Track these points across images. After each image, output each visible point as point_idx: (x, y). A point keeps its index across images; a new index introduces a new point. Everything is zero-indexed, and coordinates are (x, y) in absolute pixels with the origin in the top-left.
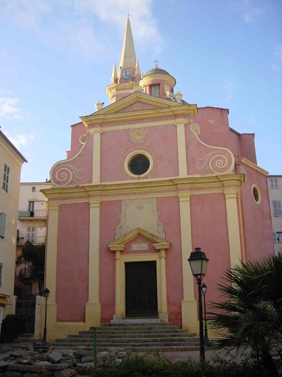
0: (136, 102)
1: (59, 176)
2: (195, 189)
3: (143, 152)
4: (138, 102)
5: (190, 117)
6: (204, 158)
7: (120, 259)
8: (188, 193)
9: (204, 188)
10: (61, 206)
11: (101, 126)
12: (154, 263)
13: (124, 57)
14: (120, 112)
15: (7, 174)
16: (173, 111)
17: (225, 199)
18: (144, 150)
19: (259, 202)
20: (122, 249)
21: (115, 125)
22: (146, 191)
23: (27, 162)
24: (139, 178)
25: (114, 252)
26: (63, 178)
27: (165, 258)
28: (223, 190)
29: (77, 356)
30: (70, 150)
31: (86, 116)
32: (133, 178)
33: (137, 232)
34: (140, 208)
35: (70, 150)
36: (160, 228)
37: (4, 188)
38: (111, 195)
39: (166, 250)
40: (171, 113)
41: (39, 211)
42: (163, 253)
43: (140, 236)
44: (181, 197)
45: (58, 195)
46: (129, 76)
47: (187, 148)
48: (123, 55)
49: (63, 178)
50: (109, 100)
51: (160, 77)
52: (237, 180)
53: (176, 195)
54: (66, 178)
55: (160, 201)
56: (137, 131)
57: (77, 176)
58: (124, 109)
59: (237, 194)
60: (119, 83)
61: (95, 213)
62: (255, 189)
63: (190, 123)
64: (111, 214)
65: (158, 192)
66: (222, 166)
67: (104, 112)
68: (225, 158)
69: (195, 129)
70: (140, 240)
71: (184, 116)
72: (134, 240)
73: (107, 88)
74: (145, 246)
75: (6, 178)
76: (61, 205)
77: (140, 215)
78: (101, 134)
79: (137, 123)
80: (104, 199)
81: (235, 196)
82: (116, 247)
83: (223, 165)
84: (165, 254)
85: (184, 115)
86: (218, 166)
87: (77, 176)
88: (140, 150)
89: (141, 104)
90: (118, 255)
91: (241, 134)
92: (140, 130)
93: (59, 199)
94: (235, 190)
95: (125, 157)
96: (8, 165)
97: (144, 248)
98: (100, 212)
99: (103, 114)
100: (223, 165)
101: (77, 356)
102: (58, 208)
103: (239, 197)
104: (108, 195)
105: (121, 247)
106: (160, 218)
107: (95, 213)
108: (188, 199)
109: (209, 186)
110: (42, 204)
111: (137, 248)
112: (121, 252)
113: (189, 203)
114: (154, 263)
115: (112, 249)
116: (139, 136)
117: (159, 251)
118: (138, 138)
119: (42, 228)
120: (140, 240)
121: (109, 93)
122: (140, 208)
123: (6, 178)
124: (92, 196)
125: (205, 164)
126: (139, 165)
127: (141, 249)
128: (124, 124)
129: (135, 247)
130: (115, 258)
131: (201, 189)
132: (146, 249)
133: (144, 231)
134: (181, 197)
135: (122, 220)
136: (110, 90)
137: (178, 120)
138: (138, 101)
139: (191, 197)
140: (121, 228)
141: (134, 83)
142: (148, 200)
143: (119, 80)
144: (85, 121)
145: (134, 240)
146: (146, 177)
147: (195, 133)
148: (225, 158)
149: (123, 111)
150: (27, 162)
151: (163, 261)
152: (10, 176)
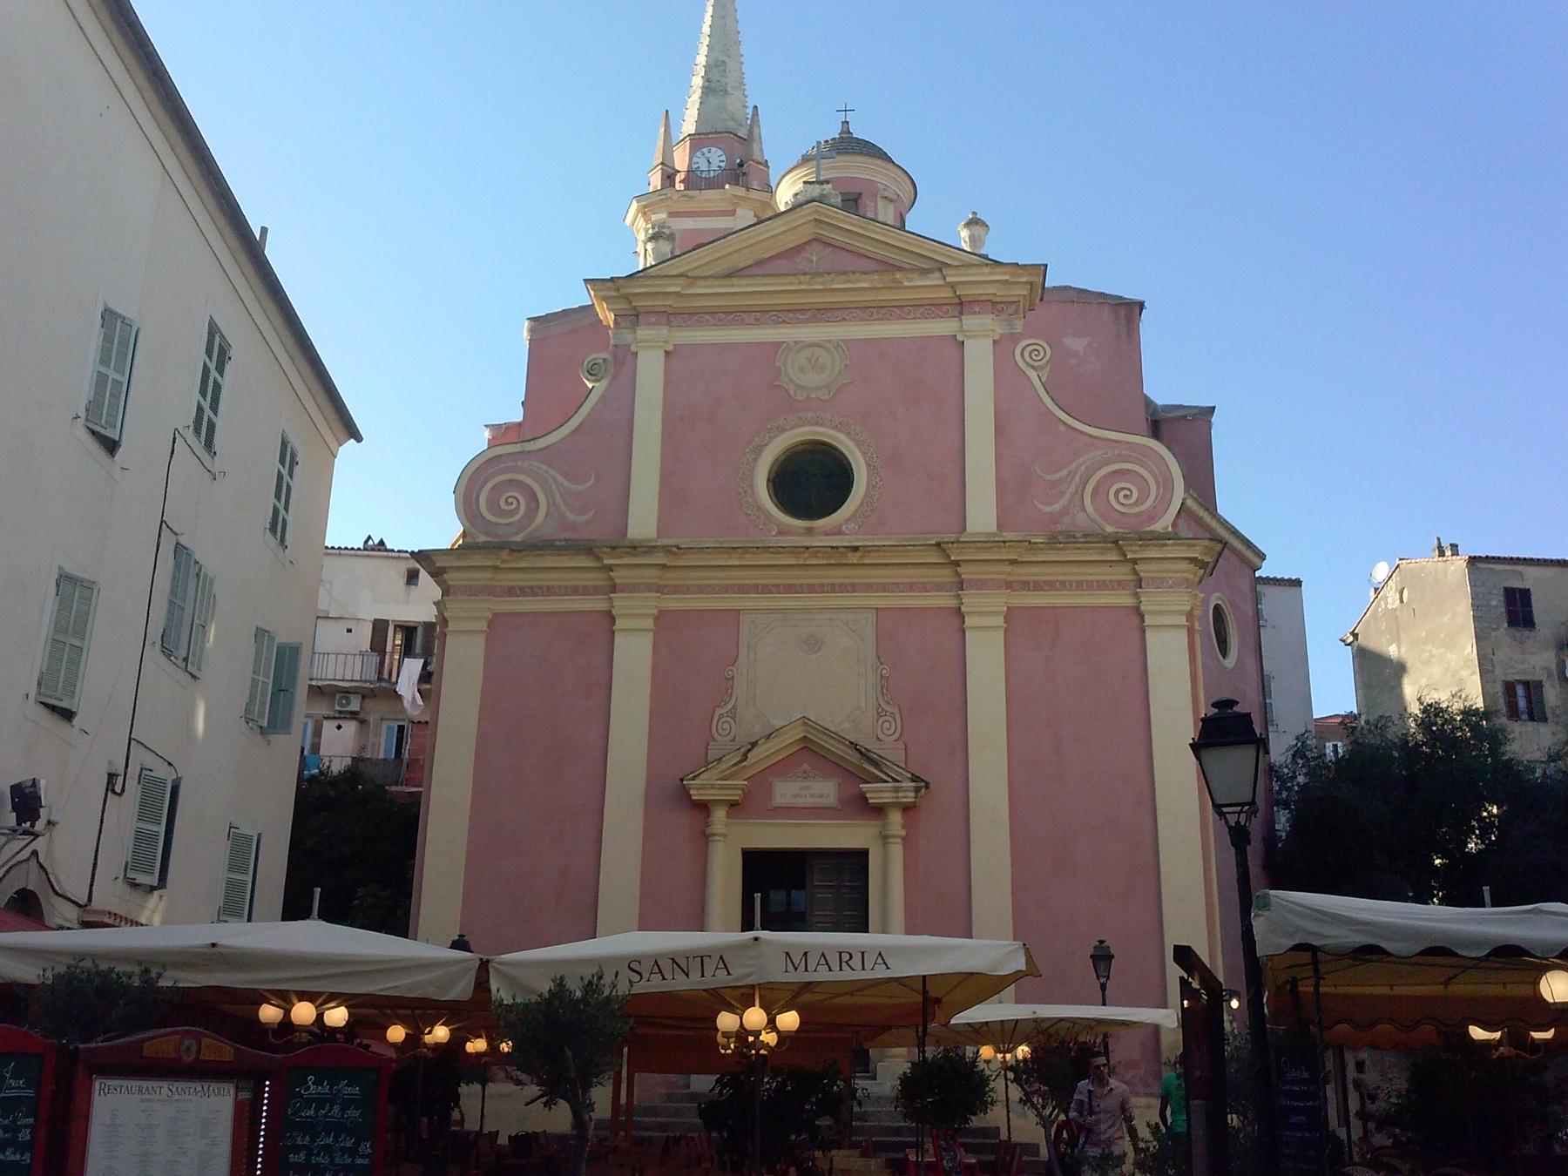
1: (493, 505)
2: (1025, 585)
3: (823, 434)
4: (814, 255)
5: (1016, 312)
6: (1065, 472)
7: (725, 836)
8: (1000, 601)
9: (1063, 583)
10: (496, 619)
11: (669, 323)
13: (703, 87)
14: (745, 272)
15: (286, 477)
16: (952, 286)
18: (836, 428)
19: (1230, 662)
20: (735, 796)
21: (722, 324)
22: (838, 581)
23: (359, 439)
24: (810, 532)
25: (704, 808)
26: (501, 513)
27: (903, 839)
28: (1137, 595)
30: (517, 416)
31: (612, 279)
33: (798, 733)
34: (813, 644)
35: (517, 416)
36: (886, 725)
37: (273, 529)
38: (701, 590)
39: (907, 809)
40: (946, 294)
41: (332, 657)
42: (896, 817)
43: (812, 751)
45: (489, 575)
46: (732, 155)
47: (999, 430)
48: (697, 81)
49: (501, 513)
50: (633, 250)
51: (855, 168)
52: (1193, 560)
53: (953, 603)
54: (516, 518)
55: (889, 626)
56: (807, 352)
57: (563, 507)
58: (760, 263)
59: (1190, 615)
60: (679, 186)
61: (634, 656)
62: (1217, 609)
63: (1014, 339)
64: (696, 662)
65: (884, 587)
67: (681, 270)
68: (1147, 475)
69: (1033, 357)
70: (806, 767)
71: (994, 306)
72: (783, 767)
73: (635, 205)
74: (825, 790)
75: (282, 490)
76: (496, 615)
77: (809, 666)
78: (667, 353)
79: (808, 321)
80: (673, 603)
81: (1183, 620)
82: (713, 787)
83: (1137, 503)
84: (904, 827)
85: (995, 304)
86: (1118, 507)
87: (563, 507)
88: (817, 424)
89: (829, 250)
90: (719, 815)
92: (818, 351)
93: (491, 591)
94: (1181, 601)
95: (758, 450)
96: (294, 441)
98: (655, 648)
99: (681, 275)
100: (1137, 503)
102: (484, 626)
103: (1197, 626)
104: (688, 590)
105: (735, 788)
106: (885, 686)
107: (634, 656)
108: (1000, 621)
109: (1081, 578)
110: (349, 631)
113: (1000, 636)
115: (696, 795)
116: (817, 365)
117: (879, 811)
118: (813, 379)
120: (806, 767)
121: (641, 223)
122: (813, 644)
123: (282, 490)
124: (627, 588)
125: (1068, 495)
126: (812, 481)
127: (808, 801)
128: (758, 323)
129: (786, 791)
130: (708, 831)
131: (1051, 585)
133: (825, 731)
136: (644, 214)
137: (970, 321)
138: (817, 240)
139: (1010, 614)
140: (733, 714)
141: (741, 191)
143: (678, 178)
144: (604, 299)
145: (783, 767)
147: (1032, 374)
148: (1147, 475)
149: (755, 271)
150: (359, 439)
151: (897, 851)
152: (299, 482)
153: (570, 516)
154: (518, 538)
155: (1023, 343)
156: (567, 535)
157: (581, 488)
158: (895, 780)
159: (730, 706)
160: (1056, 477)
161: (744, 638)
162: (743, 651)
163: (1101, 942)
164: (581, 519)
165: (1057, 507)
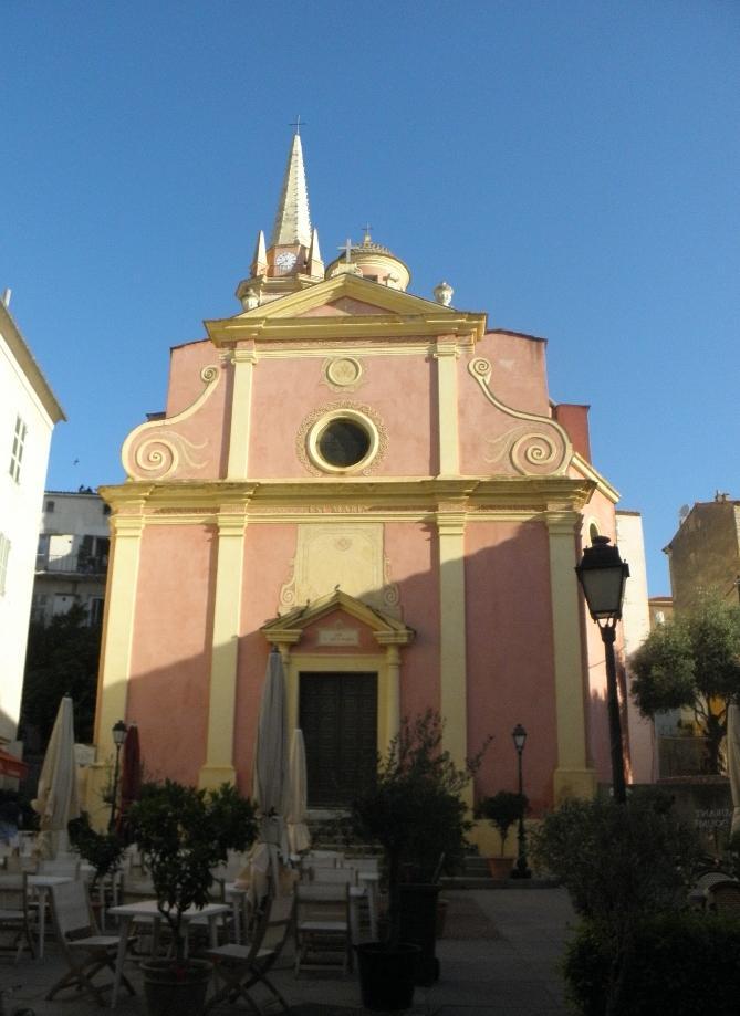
0: (342, 298)
6: (500, 439)
12: (372, 678)
17: (547, 538)
20: (294, 639)
23: (64, 419)
24: (342, 474)
29: (307, 253)
32: (333, 475)
42: (392, 655)
44: (443, 526)
66: (543, 459)
74: (351, 636)
91: (46, 529)
96: (25, 420)
97: (348, 639)
101: (307, 253)
111: (332, 639)
112: (292, 646)
114: (372, 678)
117: (383, 648)
119: (67, 598)
120: (339, 621)
122: (344, 544)
125: (502, 453)
129: (326, 636)
132: (355, 642)
134: (443, 526)
135: (298, 575)
140: (293, 588)
142: (364, 527)
146: (361, 474)
153: (193, 465)
154: (160, 479)
155: (474, 360)
156: (189, 477)
157: (202, 446)
158: (395, 629)
159: (290, 584)
160: (495, 442)
161: (300, 542)
162: (299, 549)
163: (519, 726)
164: (199, 467)
165: (496, 460)
